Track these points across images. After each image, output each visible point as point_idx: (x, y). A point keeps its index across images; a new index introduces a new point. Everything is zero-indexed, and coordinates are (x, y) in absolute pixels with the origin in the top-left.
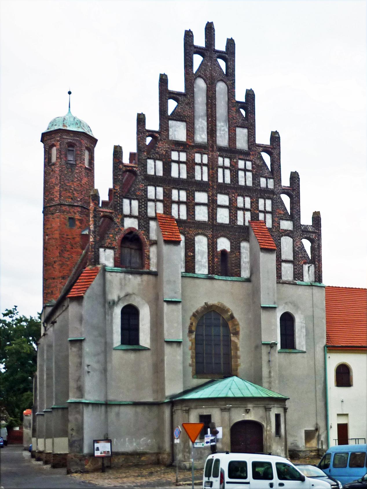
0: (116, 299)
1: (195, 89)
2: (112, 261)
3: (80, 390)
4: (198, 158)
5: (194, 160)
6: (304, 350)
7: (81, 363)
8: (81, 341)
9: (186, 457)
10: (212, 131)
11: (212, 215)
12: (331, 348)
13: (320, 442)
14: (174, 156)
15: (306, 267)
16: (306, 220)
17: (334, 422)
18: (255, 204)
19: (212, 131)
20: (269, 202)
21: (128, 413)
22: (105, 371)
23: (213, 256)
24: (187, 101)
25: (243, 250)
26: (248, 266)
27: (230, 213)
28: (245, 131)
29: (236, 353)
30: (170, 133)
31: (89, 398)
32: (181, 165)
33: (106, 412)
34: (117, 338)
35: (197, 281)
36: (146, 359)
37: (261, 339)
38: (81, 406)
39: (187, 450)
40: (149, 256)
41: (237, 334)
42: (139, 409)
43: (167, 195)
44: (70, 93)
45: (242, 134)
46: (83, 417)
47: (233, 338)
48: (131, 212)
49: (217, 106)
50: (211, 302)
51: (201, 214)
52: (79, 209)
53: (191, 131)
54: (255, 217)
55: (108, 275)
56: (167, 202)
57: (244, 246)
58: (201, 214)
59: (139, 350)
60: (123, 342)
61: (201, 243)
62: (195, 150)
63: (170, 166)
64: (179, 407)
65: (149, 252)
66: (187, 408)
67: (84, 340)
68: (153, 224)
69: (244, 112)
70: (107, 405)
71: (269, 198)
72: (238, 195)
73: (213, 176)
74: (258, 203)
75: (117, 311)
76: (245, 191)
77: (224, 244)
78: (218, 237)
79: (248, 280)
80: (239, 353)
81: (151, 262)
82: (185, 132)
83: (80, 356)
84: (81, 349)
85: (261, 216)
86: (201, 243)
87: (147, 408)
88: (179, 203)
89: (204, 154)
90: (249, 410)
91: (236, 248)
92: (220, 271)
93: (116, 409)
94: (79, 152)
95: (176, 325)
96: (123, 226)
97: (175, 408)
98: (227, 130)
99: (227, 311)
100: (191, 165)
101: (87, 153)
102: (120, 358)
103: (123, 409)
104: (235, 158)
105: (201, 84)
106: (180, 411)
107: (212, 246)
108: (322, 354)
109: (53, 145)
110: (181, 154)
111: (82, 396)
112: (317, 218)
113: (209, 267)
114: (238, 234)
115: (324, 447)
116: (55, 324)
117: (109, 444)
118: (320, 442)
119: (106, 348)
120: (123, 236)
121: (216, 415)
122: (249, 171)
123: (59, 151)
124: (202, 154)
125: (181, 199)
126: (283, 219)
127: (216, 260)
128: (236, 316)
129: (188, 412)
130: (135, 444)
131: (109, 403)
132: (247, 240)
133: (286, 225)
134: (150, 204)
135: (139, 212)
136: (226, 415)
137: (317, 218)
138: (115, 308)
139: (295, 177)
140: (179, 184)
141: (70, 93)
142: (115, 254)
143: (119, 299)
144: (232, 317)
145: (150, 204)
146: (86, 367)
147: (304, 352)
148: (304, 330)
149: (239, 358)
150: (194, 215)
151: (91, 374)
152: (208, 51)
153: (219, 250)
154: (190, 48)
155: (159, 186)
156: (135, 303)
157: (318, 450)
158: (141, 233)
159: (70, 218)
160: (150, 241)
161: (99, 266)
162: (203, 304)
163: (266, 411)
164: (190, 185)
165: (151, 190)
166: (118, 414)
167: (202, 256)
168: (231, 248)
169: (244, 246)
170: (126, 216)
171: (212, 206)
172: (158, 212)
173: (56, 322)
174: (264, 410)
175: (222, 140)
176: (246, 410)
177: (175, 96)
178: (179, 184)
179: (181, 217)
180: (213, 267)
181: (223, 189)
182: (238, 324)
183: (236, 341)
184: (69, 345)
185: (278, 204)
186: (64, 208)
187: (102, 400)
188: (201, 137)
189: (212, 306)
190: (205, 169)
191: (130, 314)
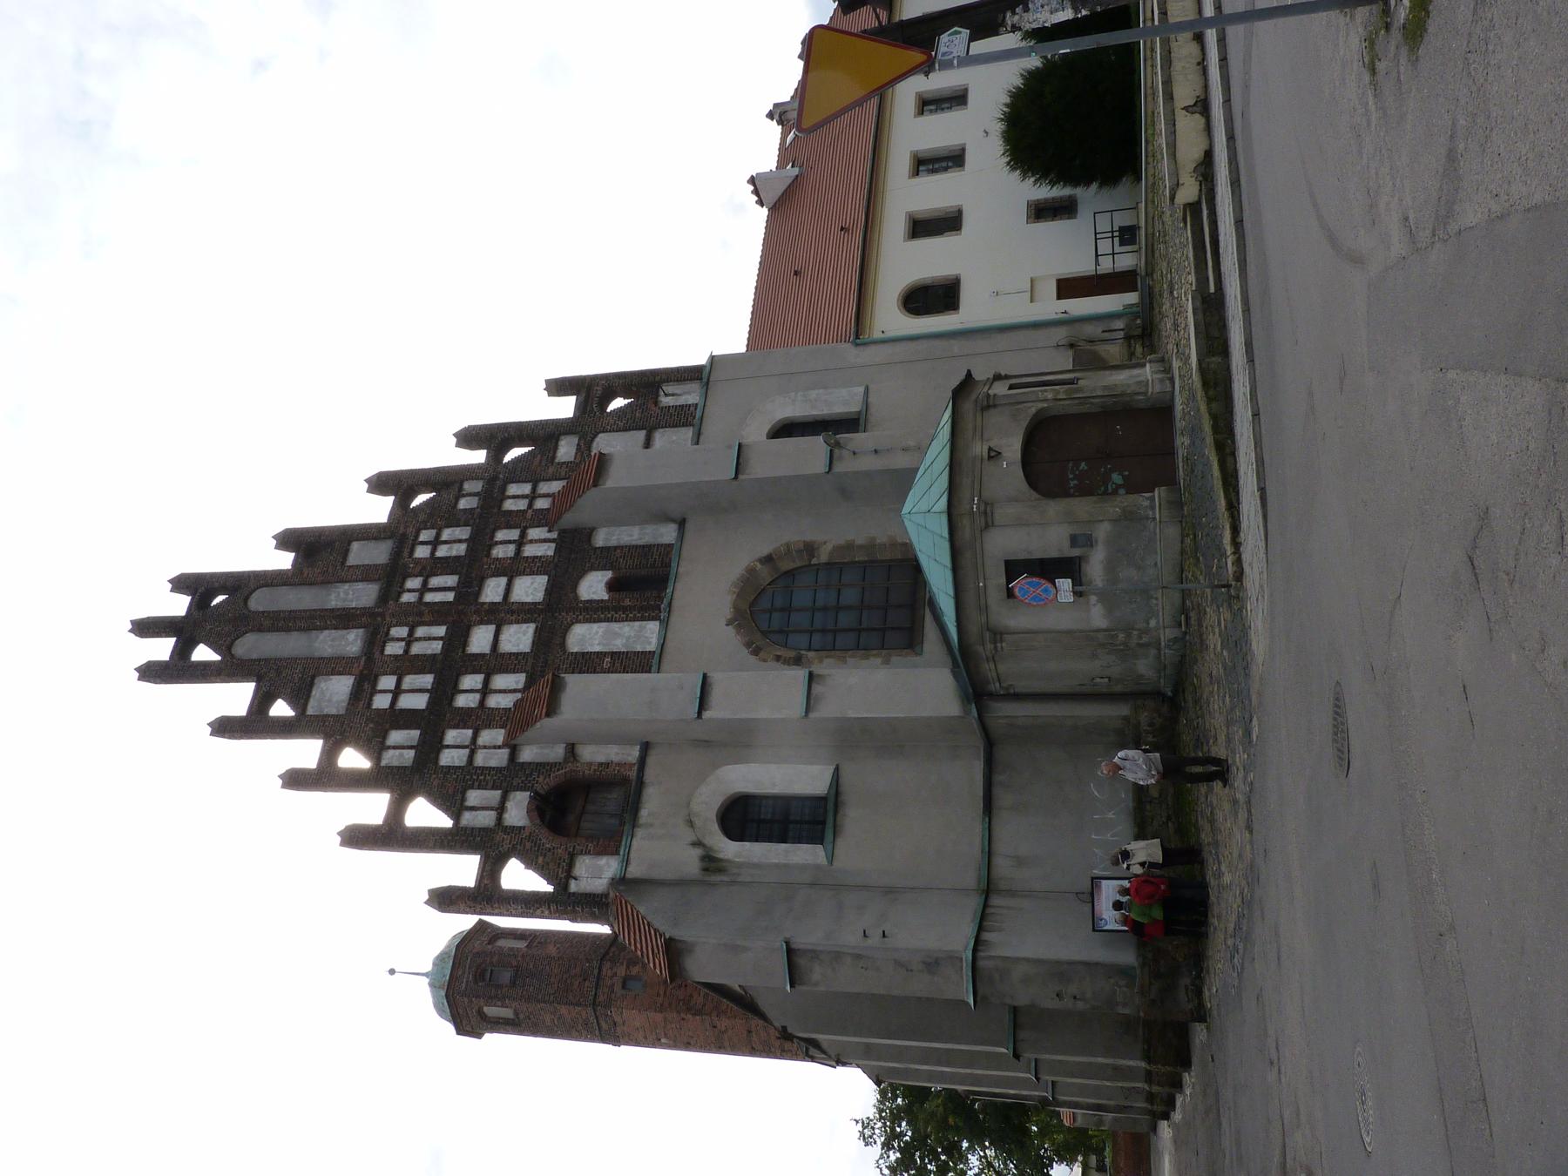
0: (698, 852)
1: (254, 656)
2: (603, 861)
3: (933, 964)
4: (394, 649)
5: (396, 657)
6: (862, 389)
7: (858, 957)
8: (790, 952)
9: (1145, 640)
10: (344, 619)
11: (523, 612)
12: (858, 330)
13: (1107, 335)
14: (381, 702)
15: (666, 401)
16: (564, 407)
17: (1051, 307)
18: (511, 520)
19: (344, 619)
20: (513, 489)
21: (1014, 834)
22: (890, 892)
23: (616, 609)
24: (272, 674)
25: (613, 542)
26: (649, 529)
27: (523, 573)
28: (355, 546)
29: (861, 547)
30: (334, 711)
31: (957, 936)
32: (405, 686)
33: (1012, 893)
34: (804, 854)
35: (670, 645)
36: (865, 776)
37: (817, 476)
38: (981, 963)
39: (1121, 636)
40: (601, 764)
41: (810, 548)
42: (1003, 798)
43: (465, 718)
44: (392, 972)
45: (360, 554)
46: (1018, 960)
47: (823, 556)
48: (492, 809)
49: (293, 607)
50: (727, 611)
51: (518, 638)
52: (607, 965)
53: (335, 666)
54: (542, 518)
55: (634, 871)
56: (479, 718)
57: (601, 539)
58: (518, 638)
59: (837, 794)
60: (816, 838)
61: (585, 637)
62: (377, 655)
63: (402, 710)
64: (987, 669)
65: (590, 764)
66: (987, 635)
67: (787, 943)
68: (527, 755)
69: (316, 549)
70: (988, 889)
71: (503, 489)
72: (488, 555)
73: (437, 614)
74: (511, 512)
75: (730, 849)
76: (480, 543)
77: (594, 586)
78: (576, 597)
79: (682, 524)
80: (860, 541)
81: (616, 759)
82: (335, 678)
83: (837, 956)
84: (814, 954)
85: (542, 504)
86: (585, 637)
87: (998, 778)
88: (485, 691)
89: (387, 633)
90: (990, 449)
91: (606, 558)
92: (655, 593)
93: (1002, 866)
94: (495, 959)
95: (766, 691)
96: (521, 828)
97: (994, 687)
98: (346, 586)
99: (751, 571)
100: (407, 665)
101: (501, 943)
102: (860, 845)
103: (1001, 847)
104: (405, 566)
105: (250, 645)
106: (1002, 668)
107: (594, 612)
108: (872, 349)
109: (481, 1013)
110: (380, 686)
111: (954, 959)
112: (558, 387)
113: (643, 619)
114: (575, 552)
115: (1119, 324)
116: (790, 1030)
117: (1104, 882)
118: (1107, 335)
119: (825, 883)
120: (544, 831)
121: (1005, 542)
122: (438, 535)
123: (491, 1000)
124: (387, 638)
125: (479, 686)
126: (554, 457)
127: (627, 602)
128: (765, 550)
129: (997, 635)
130: (1110, 815)
131: (984, 885)
132: (589, 533)
133: (566, 450)
134: (480, 760)
135: (494, 788)
136: (1002, 513)
137: (558, 387)
138: (721, 856)
139: (468, 438)
140: (443, 692)
141: (392, 972)
142: (588, 853)
143: (698, 844)
144: (768, 560)
145: (480, 760)
146: (869, 941)
147: (867, 389)
148: (813, 394)
149: (874, 539)
150: (517, 655)
151: (887, 927)
152: (184, 631)
153: (606, 597)
154: (176, 670)
155: (442, 738)
156: (716, 803)
157: (1128, 338)
158: (544, 783)
159: (624, 987)
160: (566, 760)
161: (612, 895)
162: (731, 630)
163: (995, 406)
164: (448, 667)
165: (449, 758)
166: (1020, 861)
167: (617, 635)
168: (604, 568)
169: (601, 539)
170: (500, 819)
171: (503, 614)
172: (500, 743)
173: (784, 1028)
174: (992, 411)
175: (362, 595)
176: (990, 457)
177: (261, 702)
178: (443, 692)
179: (521, 686)
180: (641, 609)
181: (469, 589)
182: (788, 545)
183: (829, 547)
184: (804, 988)
185: (520, 470)
186: (601, 998)
187: (973, 903)
188: (351, 642)
189: (737, 610)
190: (421, 631)
191: (743, 817)
